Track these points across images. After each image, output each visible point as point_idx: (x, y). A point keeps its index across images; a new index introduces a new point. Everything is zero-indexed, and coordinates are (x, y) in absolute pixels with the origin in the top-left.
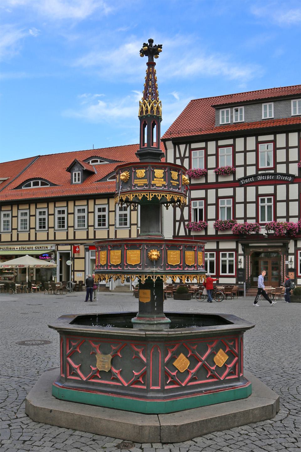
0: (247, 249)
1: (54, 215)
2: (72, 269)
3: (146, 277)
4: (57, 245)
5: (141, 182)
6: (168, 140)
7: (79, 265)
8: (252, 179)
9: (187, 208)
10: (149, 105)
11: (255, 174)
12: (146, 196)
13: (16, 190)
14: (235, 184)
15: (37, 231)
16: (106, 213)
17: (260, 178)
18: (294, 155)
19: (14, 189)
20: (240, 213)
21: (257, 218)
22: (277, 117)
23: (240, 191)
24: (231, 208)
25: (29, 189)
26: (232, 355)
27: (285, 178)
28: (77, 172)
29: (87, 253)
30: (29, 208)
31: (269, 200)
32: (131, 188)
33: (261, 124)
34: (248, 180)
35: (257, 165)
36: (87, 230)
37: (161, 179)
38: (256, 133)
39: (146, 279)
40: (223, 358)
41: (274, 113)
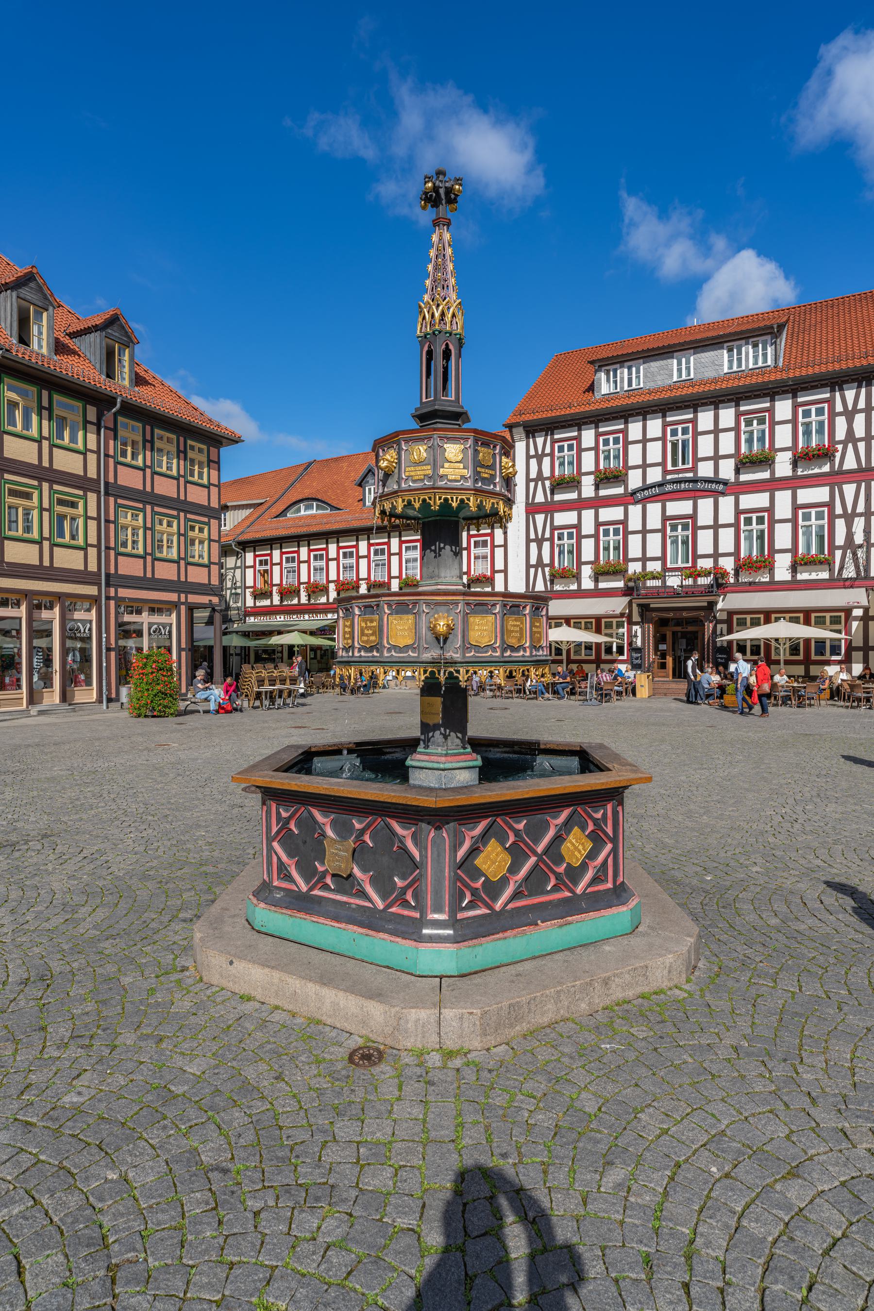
3: (425, 672)
5: (419, 473)
6: (517, 425)
9: (548, 543)
12: (428, 501)
14: (630, 498)
17: (669, 488)
20: (634, 551)
21: (663, 559)
22: (699, 376)
23: (635, 511)
26: (597, 839)
32: (399, 485)
35: (663, 464)
37: (458, 464)
39: (426, 678)
40: (580, 847)
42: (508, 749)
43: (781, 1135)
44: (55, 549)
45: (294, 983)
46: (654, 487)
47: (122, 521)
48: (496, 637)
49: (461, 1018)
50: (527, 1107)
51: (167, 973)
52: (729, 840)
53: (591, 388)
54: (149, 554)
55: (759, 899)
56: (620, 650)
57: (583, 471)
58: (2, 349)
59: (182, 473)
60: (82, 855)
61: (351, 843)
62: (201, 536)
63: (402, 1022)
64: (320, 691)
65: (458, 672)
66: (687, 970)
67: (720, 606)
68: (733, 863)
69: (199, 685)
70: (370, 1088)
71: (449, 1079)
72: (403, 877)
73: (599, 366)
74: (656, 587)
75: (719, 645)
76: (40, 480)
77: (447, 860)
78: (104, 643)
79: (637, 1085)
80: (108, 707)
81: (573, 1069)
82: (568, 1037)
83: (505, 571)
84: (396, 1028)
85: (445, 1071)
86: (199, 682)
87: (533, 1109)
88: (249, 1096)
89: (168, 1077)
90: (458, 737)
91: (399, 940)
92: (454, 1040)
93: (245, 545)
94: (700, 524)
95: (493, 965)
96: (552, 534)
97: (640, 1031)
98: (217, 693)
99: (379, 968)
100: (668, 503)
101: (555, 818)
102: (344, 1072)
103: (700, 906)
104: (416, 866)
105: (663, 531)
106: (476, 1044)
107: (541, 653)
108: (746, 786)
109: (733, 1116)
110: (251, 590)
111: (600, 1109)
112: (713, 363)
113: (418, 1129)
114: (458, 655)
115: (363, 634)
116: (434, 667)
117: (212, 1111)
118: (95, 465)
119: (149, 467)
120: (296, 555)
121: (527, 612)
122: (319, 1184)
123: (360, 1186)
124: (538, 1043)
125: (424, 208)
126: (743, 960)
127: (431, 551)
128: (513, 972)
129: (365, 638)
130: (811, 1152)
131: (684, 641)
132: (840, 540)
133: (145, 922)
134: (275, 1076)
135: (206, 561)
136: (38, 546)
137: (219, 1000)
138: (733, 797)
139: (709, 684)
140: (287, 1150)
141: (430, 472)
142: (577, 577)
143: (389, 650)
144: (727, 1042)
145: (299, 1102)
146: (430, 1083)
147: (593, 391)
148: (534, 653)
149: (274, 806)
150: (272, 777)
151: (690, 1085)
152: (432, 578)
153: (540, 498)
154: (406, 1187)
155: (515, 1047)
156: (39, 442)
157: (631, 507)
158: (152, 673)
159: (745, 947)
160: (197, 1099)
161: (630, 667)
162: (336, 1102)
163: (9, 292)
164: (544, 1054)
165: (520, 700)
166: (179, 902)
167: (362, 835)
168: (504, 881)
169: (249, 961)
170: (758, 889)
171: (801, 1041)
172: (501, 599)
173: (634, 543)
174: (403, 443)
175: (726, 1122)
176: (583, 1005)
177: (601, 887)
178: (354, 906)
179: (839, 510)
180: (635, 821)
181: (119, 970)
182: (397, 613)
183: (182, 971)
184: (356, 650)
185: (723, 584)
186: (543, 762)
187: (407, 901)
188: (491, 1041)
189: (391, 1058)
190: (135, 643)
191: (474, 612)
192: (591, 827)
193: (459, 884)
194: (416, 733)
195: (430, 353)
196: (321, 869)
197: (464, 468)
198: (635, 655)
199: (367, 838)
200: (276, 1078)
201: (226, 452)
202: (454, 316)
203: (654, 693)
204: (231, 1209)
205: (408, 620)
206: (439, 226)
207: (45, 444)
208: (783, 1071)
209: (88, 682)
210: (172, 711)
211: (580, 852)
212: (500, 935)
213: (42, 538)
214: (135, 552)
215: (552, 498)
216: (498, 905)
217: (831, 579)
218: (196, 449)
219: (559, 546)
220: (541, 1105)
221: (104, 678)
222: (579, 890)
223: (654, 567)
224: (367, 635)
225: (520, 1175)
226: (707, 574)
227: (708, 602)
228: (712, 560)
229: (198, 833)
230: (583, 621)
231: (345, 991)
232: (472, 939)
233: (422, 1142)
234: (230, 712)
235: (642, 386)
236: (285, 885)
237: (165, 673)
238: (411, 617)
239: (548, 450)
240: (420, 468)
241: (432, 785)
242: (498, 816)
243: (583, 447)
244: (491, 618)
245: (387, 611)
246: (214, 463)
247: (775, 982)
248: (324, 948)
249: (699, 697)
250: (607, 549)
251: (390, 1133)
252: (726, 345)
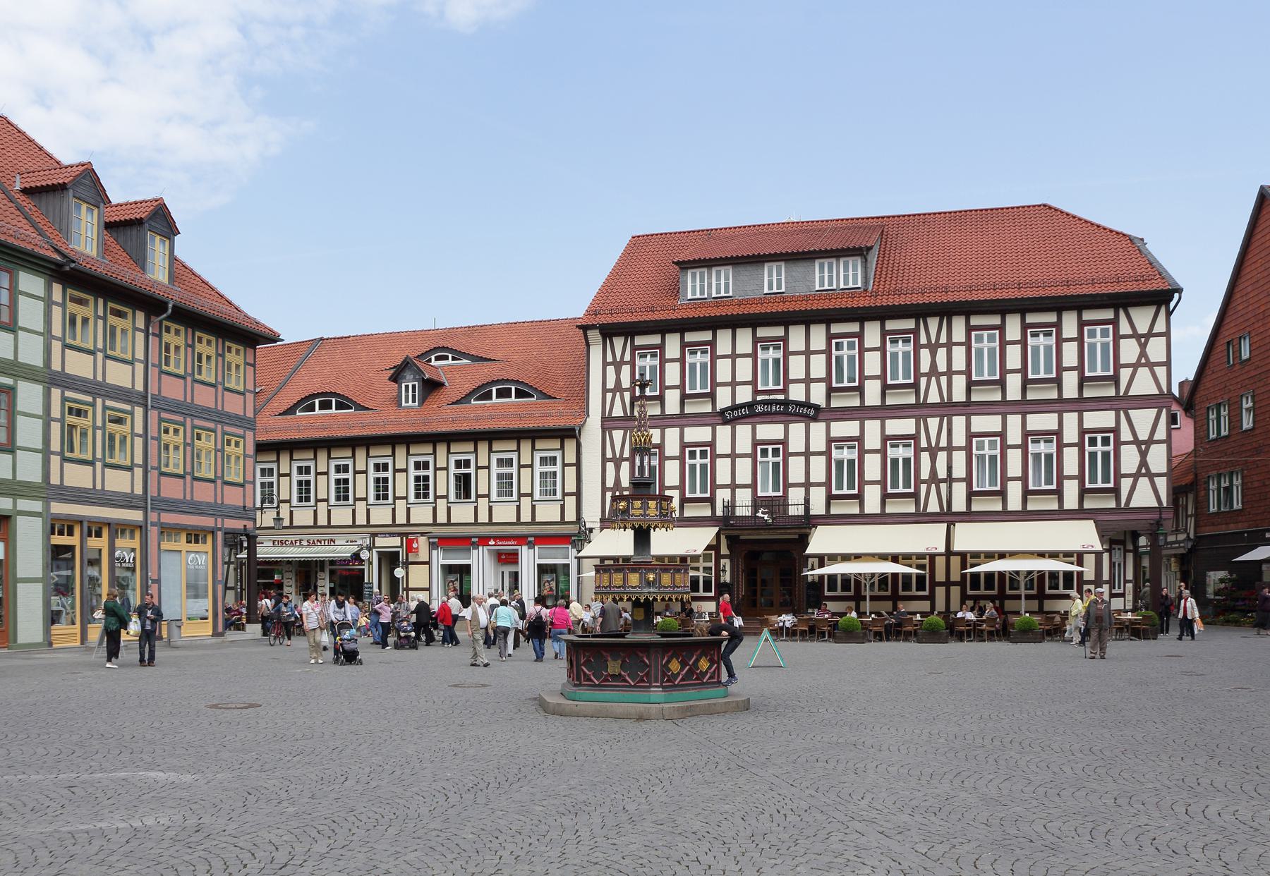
1: (531, 466)
2: (405, 586)
4: (374, 535)
6: (593, 327)
7: (417, 576)
8: (745, 411)
13: (285, 416)
15: (370, 505)
16: (430, 473)
17: (759, 409)
19: (280, 414)
23: (724, 432)
24: (779, 463)
25: (311, 417)
27: (802, 411)
28: (410, 383)
29: (434, 553)
30: (518, 450)
31: (704, 455)
34: (738, 413)
35: (754, 382)
36: (434, 505)
38: (753, 322)
41: (785, 282)
75: (810, 579)
104: (648, 666)
132: (925, 474)
153: (618, 412)
168: (679, 673)
173: (723, 466)
177: (713, 680)
179: (924, 444)
217: (917, 514)
227: (800, 535)
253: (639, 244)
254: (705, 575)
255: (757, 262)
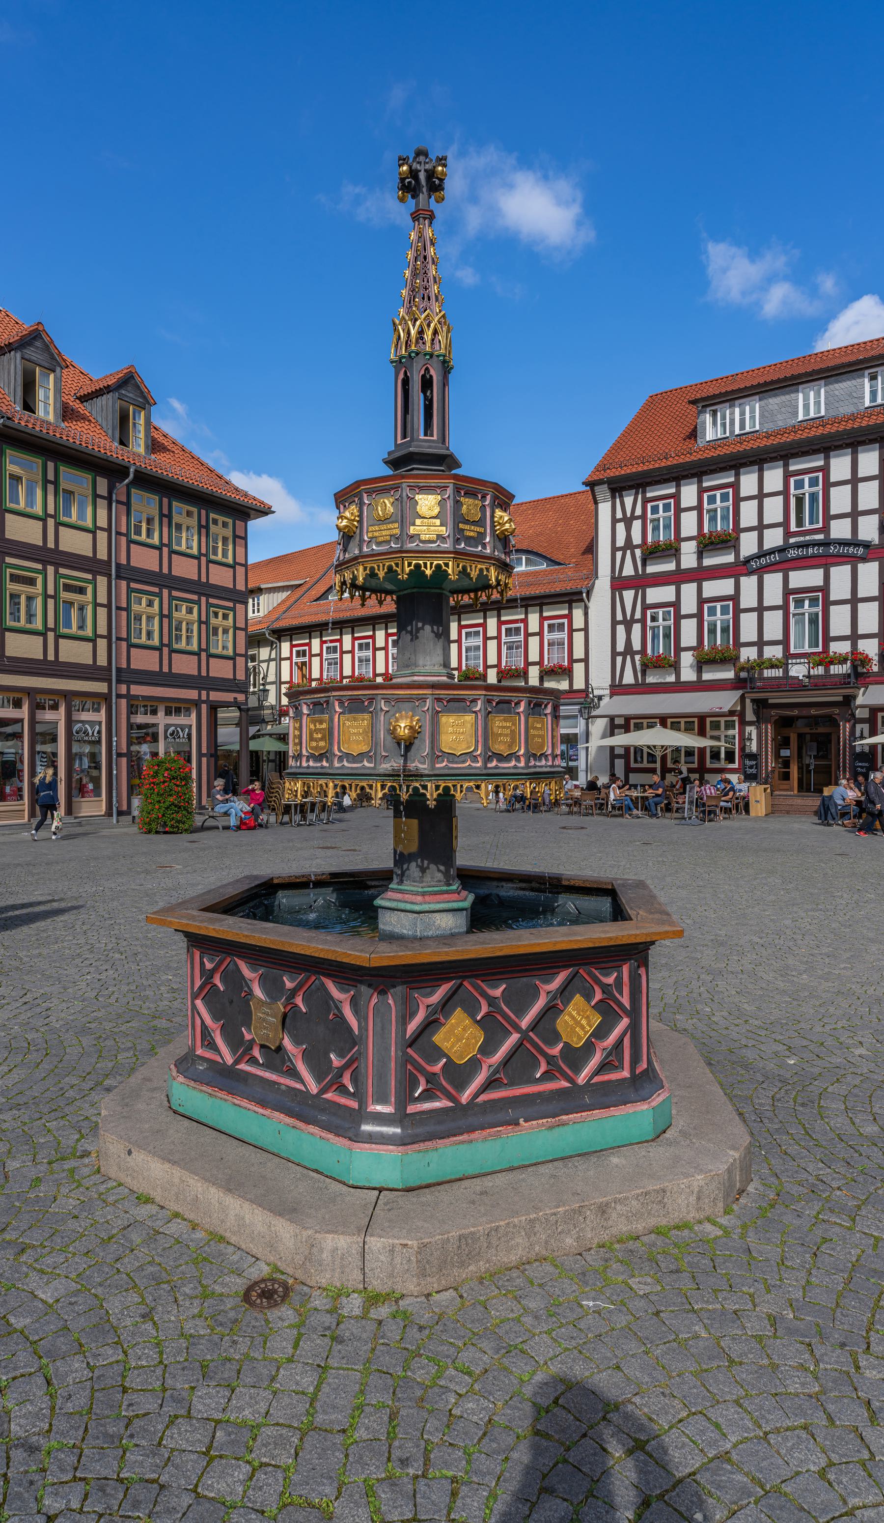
0: (765, 710)
3: (383, 787)
5: (384, 533)
8: (775, 557)
10: (414, 326)
11: (781, 543)
12: (395, 568)
17: (792, 553)
18: (869, 495)
19: (315, 601)
20: (748, 632)
22: (832, 413)
23: (749, 584)
27: (848, 550)
32: (361, 550)
33: (795, 432)
35: (786, 524)
37: (434, 520)
39: (384, 794)
40: (584, 1022)
41: (826, 404)
42: (523, 885)
43: (812, 1468)
44: (61, 641)
45: (196, 1186)
46: (774, 553)
47: (135, 607)
48: (477, 742)
49: (392, 1251)
50: (457, 1388)
51: (63, 1159)
52: (832, 1010)
53: (693, 434)
54: (166, 645)
55: (856, 1096)
56: (730, 757)
57: (683, 536)
58: (3, 417)
59: (204, 551)
60: (24, 1000)
61: (280, 1006)
62: (225, 623)
63: (315, 1250)
64: (364, 804)
65: (425, 787)
66: (727, 1196)
67: (860, 701)
68: (829, 1042)
69: (218, 797)
70: (259, 1340)
71: (364, 1336)
72: (341, 1055)
73: (703, 407)
74: (775, 678)
75: (858, 750)
76: (45, 563)
77: (393, 1035)
78: (114, 748)
79: (618, 1368)
80: (118, 822)
81: (534, 1335)
82: (541, 1286)
83: (586, 660)
84: (308, 1258)
85: (364, 1322)
86: (218, 792)
87: (463, 1391)
88: (100, 1340)
89: (13, 1303)
90: (439, 870)
91: (330, 1136)
92: (382, 1280)
93: (280, 634)
94: (832, 598)
95: (453, 1177)
96: (644, 614)
97: (642, 1284)
98: (239, 806)
99: (306, 1171)
100: (791, 573)
101: (548, 982)
102: (232, 1314)
103: (770, 1101)
105: (785, 608)
106: (411, 1287)
107: (543, 762)
108: (871, 935)
109: (747, 1430)
110: (287, 686)
111: (556, 1401)
112: (850, 395)
113: (302, 1408)
114: (425, 766)
115: (312, 739)
116: (394, 781)
117: (48, 1357)
118: (106, 545)
119: (165, 545)
120: (338, 644)
121: (521, 709)
122: (147, 1481)
123: (199, 1490)
124: (496, 1291)
125: (402, 200)
126: (813, 1185)
127: (407, 632)
128: (478, 1188)
129: (314, 744)
130: (853, 1501)
131: (815, 744)
133: (62, 1089)
134: (143, 1312)
135: (230, 652)
136: (42, 638)
137: (111, 1199)
138: (850, 949)
139: (844, 799)
140: (122, 1424)
141: (397, 531)
142: (676, 666)
143: (340, 759)
144: (764, 1309)
145: (161, 1353)
146: (337, 1339)
147: (696, 437)
148: (532, 763)
149: (197, 954)
150: (193, 918)
151: (695, 1374)
152: (408, 666)
153: (628, 570)
154: (257, 1498)
155: (465, 1295)
156: (44, 520)
157: (743, 579)
158: (164, 782)
159: (821, 1165)
160: (36, 1338)
161: (742, 777)
162: (209, 1357)
163: (12, 353)
164: (501, 1309)
165: (602, 818)
166: (110, 1065)
167: (294, 997)
169: (150, 1152)
170: (857, 1082)
171: (873, 1316)
172: (484, 693)
173: (748, 622)
174: (365, 495)
175: (734, 1439)
176: (569, 1241)
177: (614, 1076)
178: (283, 1087)
180: (710, 978)
181: (9, 1152)
182: (351, 711)
183: (82, 1157)
184: (304, 759)
185: (864, 673)
186: (569, 903)
187: (344, 1086)
188: (433, 1283)
189: (297, 1298)
190: (149, 748)
191: (448, 711)
192: (598, 996)
193: (409, 1067)
194: (390, 864)
195: (406, 382)
196: (248, 1037)
197: (442, 525)
198: (748, 763)
199: (299, 1001)
200: (143, 1316)
201: (255, 525)
202: (435, 332)
203: (773, 810)
204: (19, 1509)
205: (364, 721)
206: (418, 220)
207: (51, 522)
208: (837, 1362)
209: (97, 792)
210: (186, 826)
211: (583, 1028)
212: (465, 1137)
213: (47, 629)
214: (150, 643)
215: (644, 569)
216: (465, 1097)
218: (220, 523)
219: (653, 628)
220: (477, 1387)
221: (114, 788)
222: (582, 1078)
223: (774, 652)
224: (316, 740)
225: (418, 1496)
226: (842, 660)
227: (844, 696)
228: (849, 643)
229: (165, 977)
230: (683, 721)
231: (251, 1201)
232: (424, 1141)
233: (299, 1429)
234: (253, 828)
235: (757, 428)
236: (209, 1054)
237: (178, 783)
238: (367, 716)
239: (638, 512)
240: (385, 527)
241: (405, 931)
242: (464, 978)
243: (682, 506)
244: (469, 718)
245: (337, 709)
246: (241, 539)
247: (854, 1220)
248: (246, 1140)
249: (829, 816)
250: (712, 631)
251: (263, 1411)
252: (867, 372)
253: (655, 402)
254: (727, 745)
255: (793, 385)
